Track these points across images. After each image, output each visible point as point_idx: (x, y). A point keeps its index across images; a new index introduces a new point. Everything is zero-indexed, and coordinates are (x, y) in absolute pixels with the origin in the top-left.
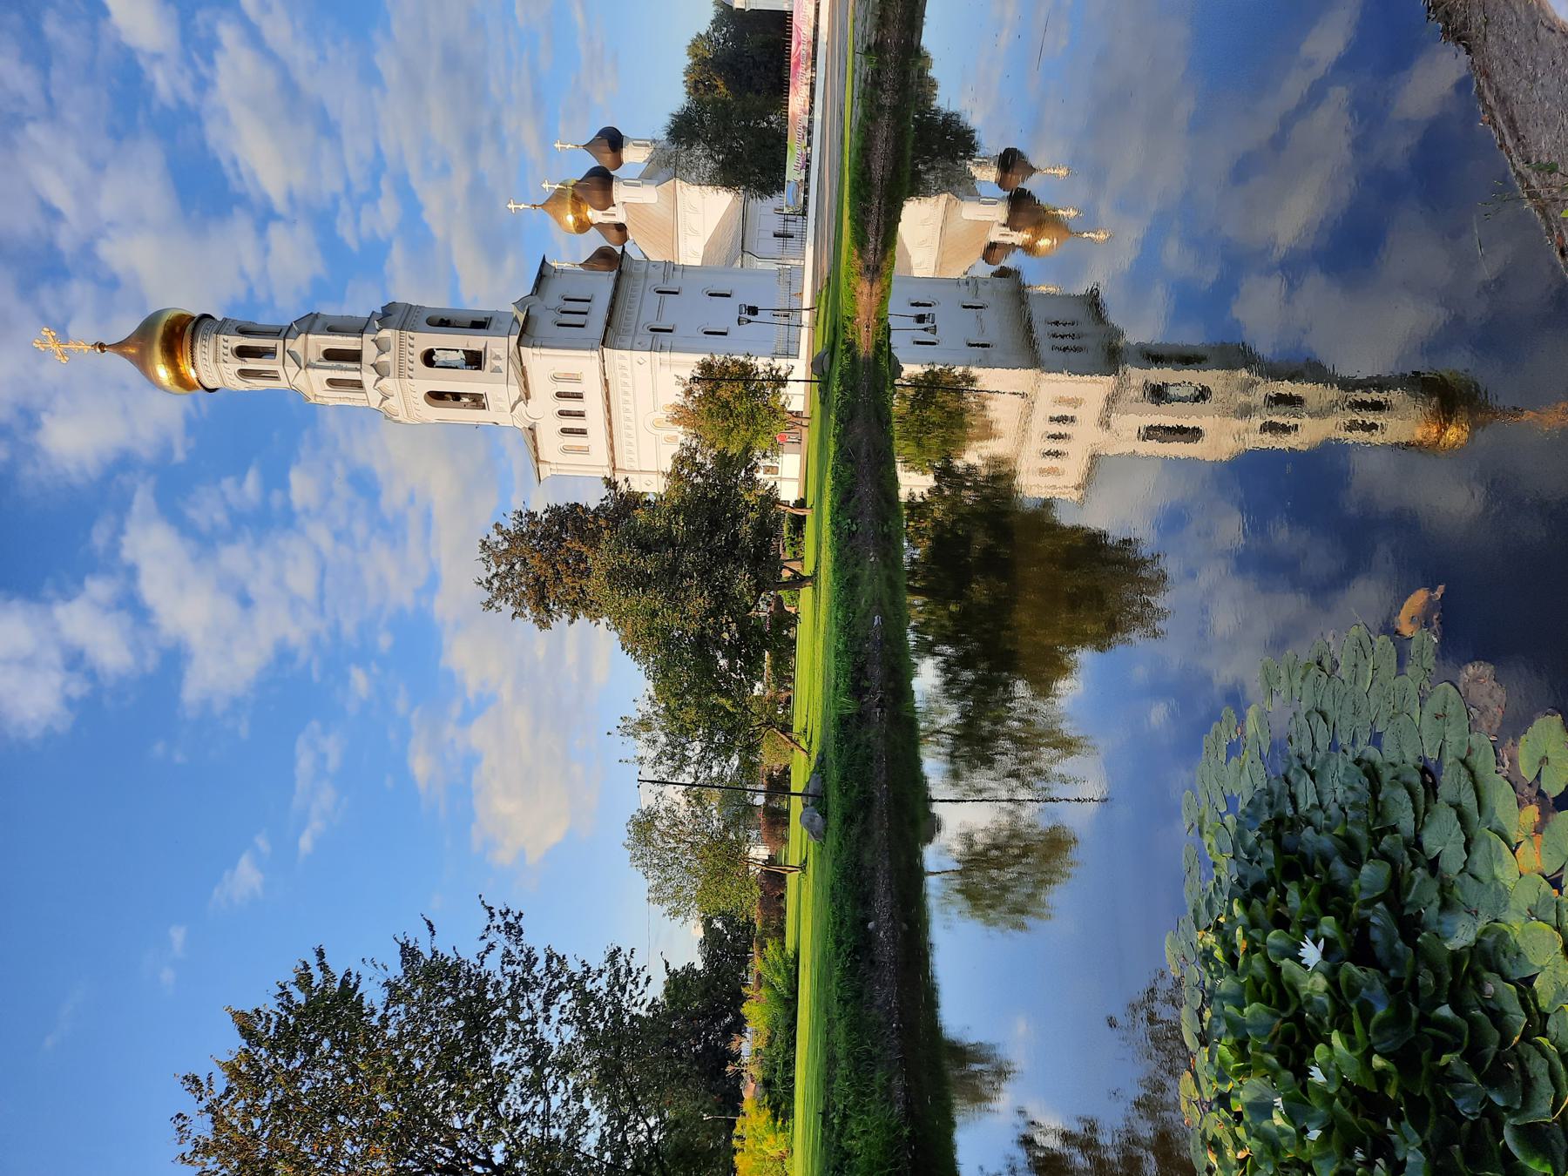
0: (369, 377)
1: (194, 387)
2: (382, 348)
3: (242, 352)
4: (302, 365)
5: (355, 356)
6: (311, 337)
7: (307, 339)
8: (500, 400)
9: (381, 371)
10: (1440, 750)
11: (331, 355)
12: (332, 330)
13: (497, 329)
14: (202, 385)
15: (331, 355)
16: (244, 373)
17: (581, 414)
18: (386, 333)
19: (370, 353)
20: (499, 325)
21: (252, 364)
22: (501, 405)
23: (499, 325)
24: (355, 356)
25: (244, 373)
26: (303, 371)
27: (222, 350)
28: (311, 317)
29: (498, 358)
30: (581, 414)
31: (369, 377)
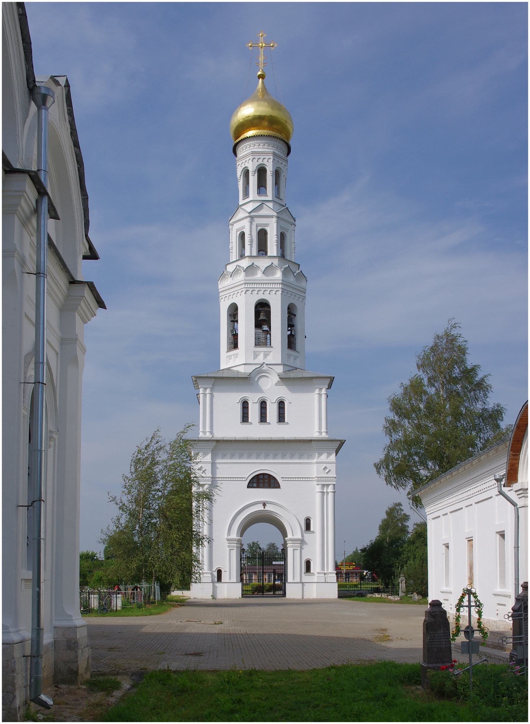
0: (245, 263)
1: (237, 137)
2: (268, 270)
3: (261, 172)
4: (252, 214)
5: (262, 248)
6: (274, 219)
7: (272, 217)
8: (266, 356)
9: (251, 269)
10: (24, 390)
11: (262, 235)
12: (282, 238)
13: (289, 356)
14: (239, 142)
15: (262, 235)
16: (246, 173)
17: (518, 495)
18: (279, 275)
19: (263, 263)
20: (292, 358)
21: (253, 180)
22: (261, 356)
23: (292, 358)
24: (262, 248)
25: (246, 173)
26: (248, 215)
27: (262, 157)
28: (293, 221)
29: (266, 356)
30: (518, 495)
31: (245, 263)
